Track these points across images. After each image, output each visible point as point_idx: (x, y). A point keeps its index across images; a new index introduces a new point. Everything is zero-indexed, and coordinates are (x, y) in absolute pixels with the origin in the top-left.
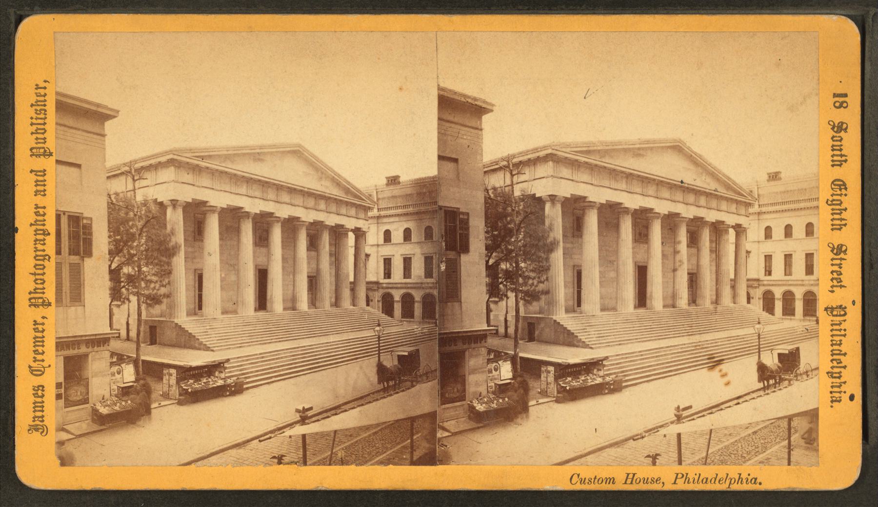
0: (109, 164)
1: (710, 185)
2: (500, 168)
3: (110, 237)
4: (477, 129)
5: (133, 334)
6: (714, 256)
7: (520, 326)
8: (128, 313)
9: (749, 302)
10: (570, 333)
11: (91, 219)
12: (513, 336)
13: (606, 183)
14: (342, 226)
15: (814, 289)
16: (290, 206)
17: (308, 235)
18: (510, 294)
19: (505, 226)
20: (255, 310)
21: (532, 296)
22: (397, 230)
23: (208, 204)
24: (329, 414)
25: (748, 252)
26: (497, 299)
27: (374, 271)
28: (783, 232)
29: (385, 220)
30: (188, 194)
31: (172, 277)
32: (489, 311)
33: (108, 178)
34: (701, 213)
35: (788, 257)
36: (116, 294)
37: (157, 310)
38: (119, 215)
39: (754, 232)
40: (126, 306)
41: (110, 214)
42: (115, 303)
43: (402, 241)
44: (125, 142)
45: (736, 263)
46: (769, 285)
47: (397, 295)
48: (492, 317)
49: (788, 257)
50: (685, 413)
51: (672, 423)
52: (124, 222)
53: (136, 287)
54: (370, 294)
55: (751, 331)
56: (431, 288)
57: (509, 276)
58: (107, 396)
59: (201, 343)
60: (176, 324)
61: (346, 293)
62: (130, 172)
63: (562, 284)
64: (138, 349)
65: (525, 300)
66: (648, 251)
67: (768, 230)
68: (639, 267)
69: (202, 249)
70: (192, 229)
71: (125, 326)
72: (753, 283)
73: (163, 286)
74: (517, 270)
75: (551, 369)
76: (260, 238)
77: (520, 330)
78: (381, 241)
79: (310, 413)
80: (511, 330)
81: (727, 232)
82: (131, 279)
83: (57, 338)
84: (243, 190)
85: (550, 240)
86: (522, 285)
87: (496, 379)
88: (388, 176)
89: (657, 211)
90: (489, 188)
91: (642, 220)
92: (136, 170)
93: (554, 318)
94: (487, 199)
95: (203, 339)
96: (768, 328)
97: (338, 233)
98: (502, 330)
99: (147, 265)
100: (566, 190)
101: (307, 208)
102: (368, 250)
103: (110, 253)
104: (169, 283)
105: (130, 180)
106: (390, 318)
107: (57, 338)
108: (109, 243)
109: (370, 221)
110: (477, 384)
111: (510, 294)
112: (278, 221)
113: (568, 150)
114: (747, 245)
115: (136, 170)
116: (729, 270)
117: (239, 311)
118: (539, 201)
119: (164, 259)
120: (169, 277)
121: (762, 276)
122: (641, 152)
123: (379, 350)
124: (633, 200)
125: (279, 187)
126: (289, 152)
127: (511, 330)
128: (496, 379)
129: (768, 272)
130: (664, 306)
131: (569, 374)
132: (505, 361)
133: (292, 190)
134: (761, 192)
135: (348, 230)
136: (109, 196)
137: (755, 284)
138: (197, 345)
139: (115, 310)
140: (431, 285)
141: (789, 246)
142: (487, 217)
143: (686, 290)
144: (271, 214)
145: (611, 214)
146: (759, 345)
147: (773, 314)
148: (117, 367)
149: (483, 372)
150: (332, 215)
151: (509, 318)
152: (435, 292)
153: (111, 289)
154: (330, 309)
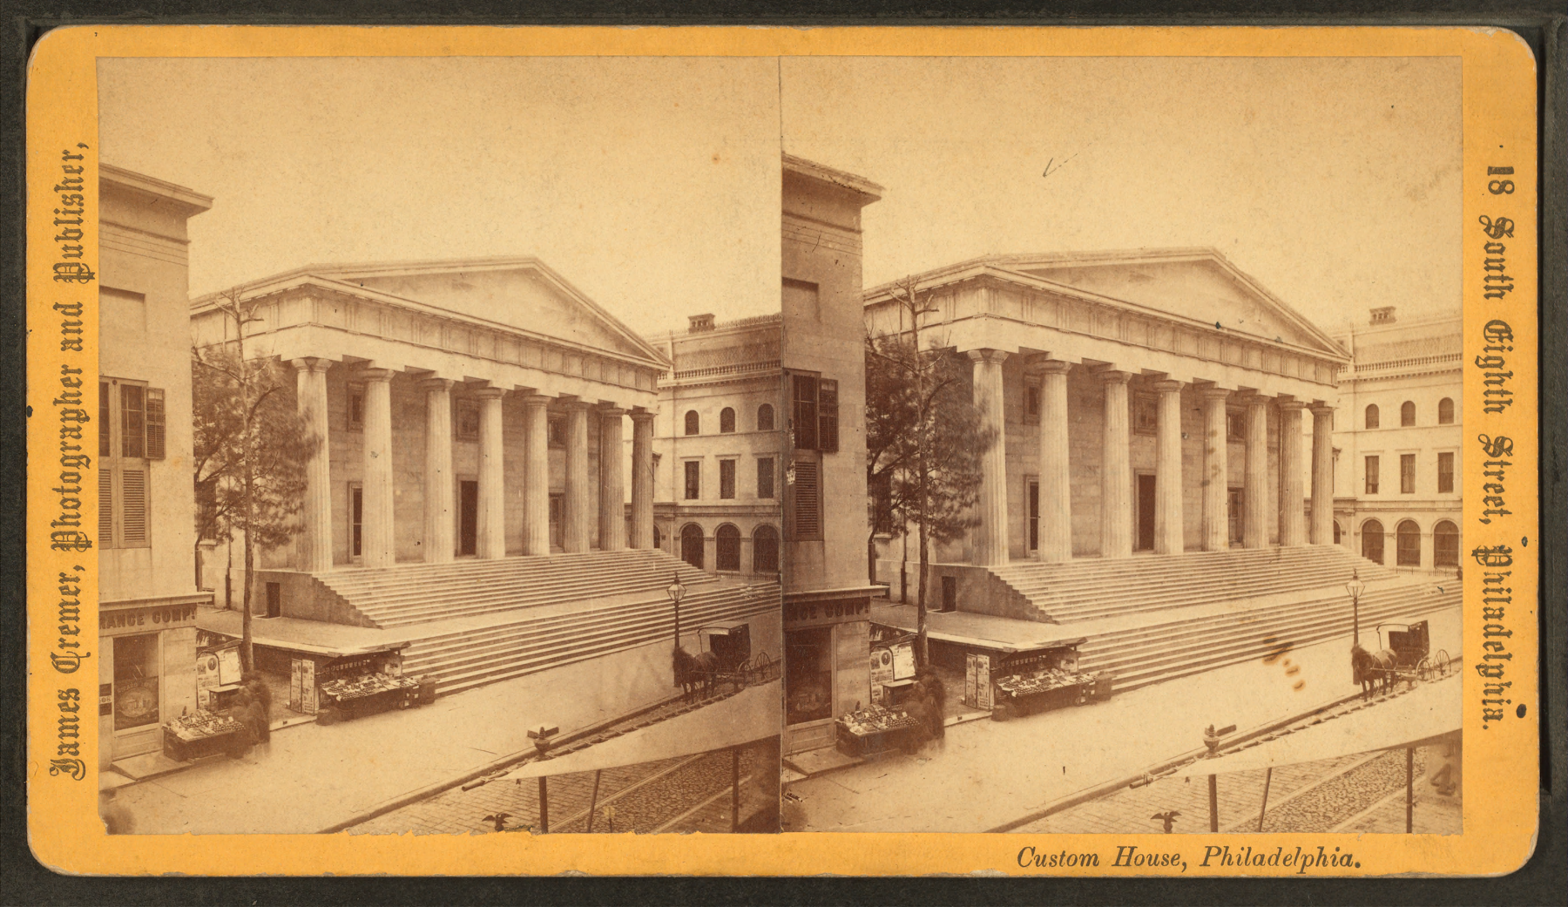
0: (195, 293)
1: (1268, 331)
2: (894, 301)
3: (196, 424)
4: (852, 230)
5: (238, 597)
6: (1275, 457)
7: (929, 582)
8: (228, 560)
9: (1337, 541)
10: (1017, 597)
11: (836, 382)
12: (917, 601)
13: (1082, 327)
14: (611, 405)
15: (1454, 517)
16: (517, 369)
17: (550, 420)
18: (910, 526)
19: (902, 405)
20: (456, 555)
21: (949, 530)
22: (708, 411)
23: (372, 365)
24: (587, 740)
25: (1336, 451)
26: (887, 535)
27: (668, 486)
28: (1398, 414)
29: (688, 394)
30: (335, 348)
31: (982, 489)
32: (873, 556)
33: (193, 318)
34: (1253, 381)
35: (1407, 461)
36: (207, 527)
37: (280, 554)
38: (213, 383)
39: (1347, 415)
40: (225, 547)
41: (196, 382)
42: (205, 542)
43: (718, 431)
44: (224, 254)
45: (1314, 472)
46: (1374, 510)
47: (709, 528)
48: (878, 568)
49: (1407, 461)
50: (1224, 739)
51: (1200, 756)
52: (222, 396)
53: (242, 514)
54: (662, 526)
55: (1340, 591)
56: (770, 515)
57: (910, 493)
58: (192, 708)
59: (359, 614)
60: (991, 574)
61: (618, 524)
62: (232, 308)
63: (1003, 508)
64: (246, 625)
65: (938, 537)
66: (480, 456)
67: (1372, 411)
68: (1141, 477)
69: (1037, 442)
70: (342, 410)
71: (899, 580)
72: (1345, 506)
73: (291, 511)
74: (924, 484)
75: (984, 659)
76: (465, 425)
77: (928, 591)
78: (681, 431)
79: (553, 740)
80: (913, 591)
81: (1298, 415)
82: (233, 499)
83: (101, 605)
84: (434, 339)
85: (981, 429)
86: (932, 510)
87: (211, 683)
88: (693, 314)
89: (1173, 377)
90: (874, 336)
91: (1147, 393)
92: (242, 305)
93: (990, 568)
94: (870, 357)
95: (362, 607)
96: (1372, 587)
97: (604, 416)
98: (896, 591)
99: (262, 474)
100: (1010, 339)
101: (1227, 365)
102: (657, 447)
103: (197, 452)
104: (302, 506)
105: (232, 321)
106: (696, 569)
107: (101, 605)
108: (195, 434)
109: (660, 396)
110: (852, 687)
111: (910, 526)
112: (496, 396)
113: (1015, 268)
114: (1335, 439)
115: (242, 305)
116: (1301, 483)
117: (427, 556)
118: (962, 360)
119: (293, 463)
120: (301, 496)
121: (1361, 494)
122: (1145, 272)
123: (677, 626)
124: (1130, 358)
125: (498, 335)
126: (516, 272)
127: (913, 591)
128: (211, 683)
129: (1372, 487)
130: (1186, 548)
131: (1016, 670)
132: (902, 645)
133: (522, 341)
134: (1359, 344)
135: (621, 412)
136: (195, 350)
137: (1349, 508)
138: (351, 617)
139: (206, 555)
140: (769, 510)
141: (1409, 440)
142: (869, 389)
143: (1226, 519)
144: (484, 384)
145: (1091, 383)
146: (1356, 617)
147: (1380, 562)
148: (210, 657)
149: (862, 665)
150: (593, 385)
151: (909, 569)
152: (777, 523)
153: (197, 517)
154: (589, 553)
